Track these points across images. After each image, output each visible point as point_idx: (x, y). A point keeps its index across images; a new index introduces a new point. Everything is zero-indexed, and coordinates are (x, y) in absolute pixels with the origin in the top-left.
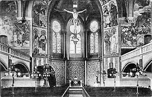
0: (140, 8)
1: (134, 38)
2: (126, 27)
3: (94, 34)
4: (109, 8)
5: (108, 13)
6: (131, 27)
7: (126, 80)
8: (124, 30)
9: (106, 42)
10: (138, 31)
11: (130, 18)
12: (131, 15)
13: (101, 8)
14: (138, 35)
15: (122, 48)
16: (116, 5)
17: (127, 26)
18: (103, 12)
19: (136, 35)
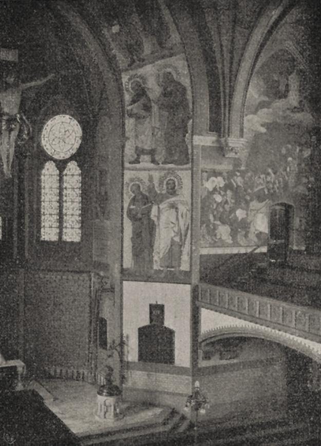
0: (262, 105)
1: (240, 214)
2: (215, 174)
3: (61, 165)
4: (154, 89)
5: (147, 108)
6: (231, 174)
7: (215, 370)
8: (209, 185)
9: (133, 217)
10: (252, 188)
11: (235, 142)
12: (235, 129)
13: (118, 80)
14: (254, 204)
15: (204, 252)
16: (186, 82)
17: (218, 168)
18: (127, 97)
19: (247, 203)
